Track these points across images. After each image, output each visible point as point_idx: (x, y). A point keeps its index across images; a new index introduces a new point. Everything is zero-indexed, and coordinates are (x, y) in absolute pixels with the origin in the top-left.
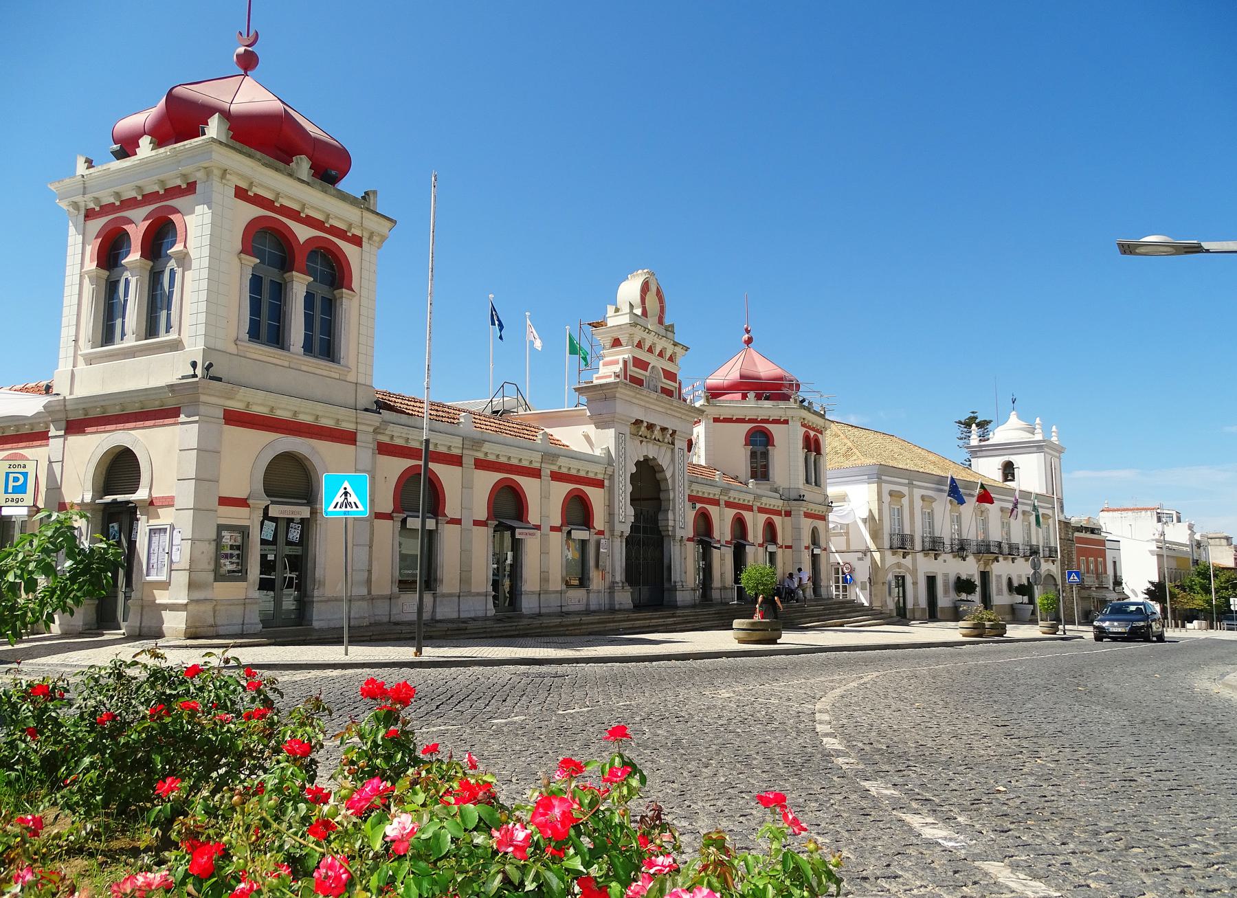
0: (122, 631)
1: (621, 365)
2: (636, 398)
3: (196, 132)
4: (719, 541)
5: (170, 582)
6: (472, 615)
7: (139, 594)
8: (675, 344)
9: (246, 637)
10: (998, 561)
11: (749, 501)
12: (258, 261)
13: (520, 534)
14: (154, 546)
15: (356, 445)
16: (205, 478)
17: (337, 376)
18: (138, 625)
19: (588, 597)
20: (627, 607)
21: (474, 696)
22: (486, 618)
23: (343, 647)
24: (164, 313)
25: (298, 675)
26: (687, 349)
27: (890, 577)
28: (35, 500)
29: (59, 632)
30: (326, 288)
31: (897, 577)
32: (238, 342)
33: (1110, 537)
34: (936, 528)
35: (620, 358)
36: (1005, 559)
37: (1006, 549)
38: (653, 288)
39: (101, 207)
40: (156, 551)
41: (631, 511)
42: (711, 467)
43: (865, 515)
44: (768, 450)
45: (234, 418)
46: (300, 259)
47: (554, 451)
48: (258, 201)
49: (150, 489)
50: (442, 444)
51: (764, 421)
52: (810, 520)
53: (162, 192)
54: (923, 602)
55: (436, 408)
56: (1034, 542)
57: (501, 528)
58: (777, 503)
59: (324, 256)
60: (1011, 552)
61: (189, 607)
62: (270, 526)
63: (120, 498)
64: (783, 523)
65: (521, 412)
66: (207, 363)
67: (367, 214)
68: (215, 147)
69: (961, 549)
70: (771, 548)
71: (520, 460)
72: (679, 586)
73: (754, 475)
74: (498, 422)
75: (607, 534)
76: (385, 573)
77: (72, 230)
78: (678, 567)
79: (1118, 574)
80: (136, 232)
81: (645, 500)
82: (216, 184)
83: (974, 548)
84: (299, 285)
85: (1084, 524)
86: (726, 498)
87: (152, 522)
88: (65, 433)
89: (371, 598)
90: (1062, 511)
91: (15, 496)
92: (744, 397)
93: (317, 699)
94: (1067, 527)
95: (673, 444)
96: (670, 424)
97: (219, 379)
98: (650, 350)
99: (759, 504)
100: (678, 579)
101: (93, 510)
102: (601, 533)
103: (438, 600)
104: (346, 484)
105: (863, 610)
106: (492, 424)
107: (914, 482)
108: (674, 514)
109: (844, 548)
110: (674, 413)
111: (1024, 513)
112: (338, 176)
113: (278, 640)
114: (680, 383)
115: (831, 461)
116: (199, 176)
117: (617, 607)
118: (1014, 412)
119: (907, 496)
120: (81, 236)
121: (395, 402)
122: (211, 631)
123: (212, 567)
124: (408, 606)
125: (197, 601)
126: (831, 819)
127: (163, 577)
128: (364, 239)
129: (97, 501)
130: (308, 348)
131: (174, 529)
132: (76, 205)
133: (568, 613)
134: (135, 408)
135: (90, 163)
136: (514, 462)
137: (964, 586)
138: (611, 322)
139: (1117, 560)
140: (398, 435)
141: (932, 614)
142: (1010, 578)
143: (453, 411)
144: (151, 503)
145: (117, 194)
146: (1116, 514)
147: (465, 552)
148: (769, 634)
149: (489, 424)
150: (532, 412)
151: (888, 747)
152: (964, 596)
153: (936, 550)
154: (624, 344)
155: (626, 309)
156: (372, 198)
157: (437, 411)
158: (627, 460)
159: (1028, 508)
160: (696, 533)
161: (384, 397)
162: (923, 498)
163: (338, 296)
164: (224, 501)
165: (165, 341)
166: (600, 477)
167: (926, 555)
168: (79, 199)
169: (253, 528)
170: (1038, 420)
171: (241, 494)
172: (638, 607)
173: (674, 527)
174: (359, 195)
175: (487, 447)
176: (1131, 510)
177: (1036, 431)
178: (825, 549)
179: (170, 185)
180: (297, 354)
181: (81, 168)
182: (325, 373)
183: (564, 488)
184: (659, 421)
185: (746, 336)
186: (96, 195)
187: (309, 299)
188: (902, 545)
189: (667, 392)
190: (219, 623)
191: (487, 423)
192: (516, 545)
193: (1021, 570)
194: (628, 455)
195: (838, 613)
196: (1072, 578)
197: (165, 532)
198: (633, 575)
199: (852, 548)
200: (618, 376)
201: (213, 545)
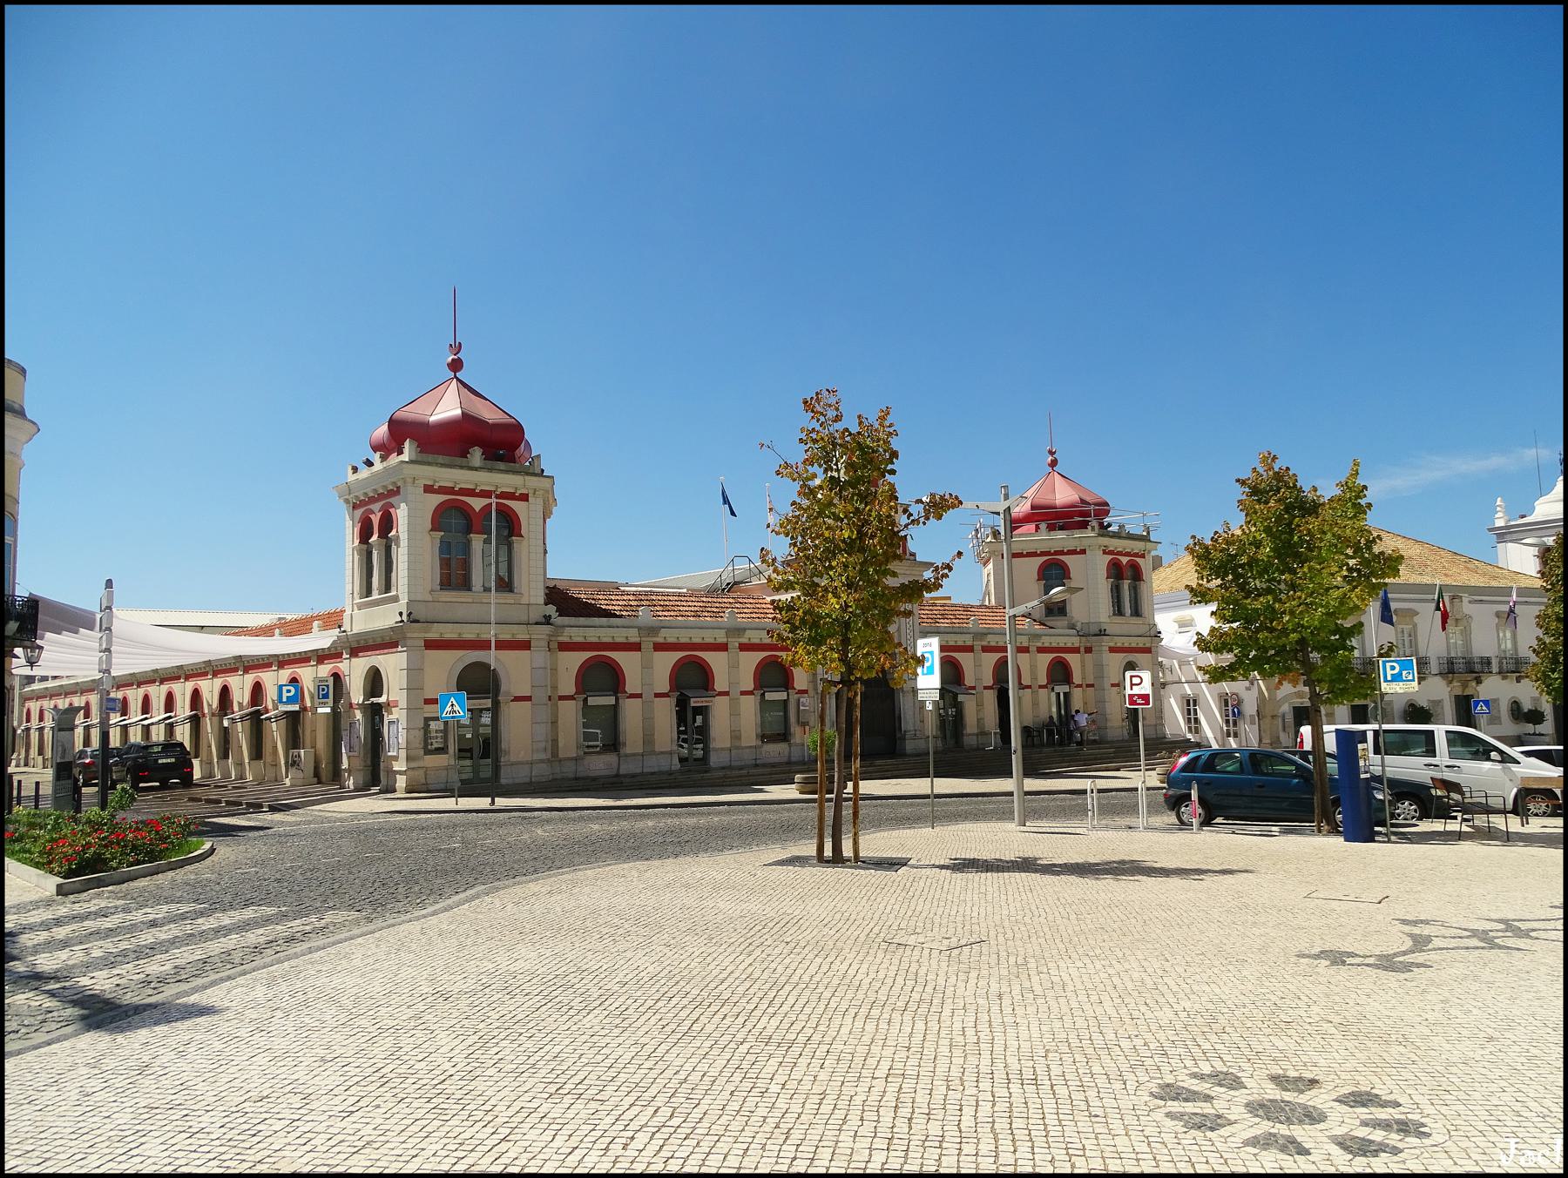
9: (447, 791)
17: (513, 602)
22: (670, 773)
34: (1420, 639)
45: (431, 645)
48: (1111, 553)
51: (1057, 553)
58: (1074, 641)
61: (408, 773)
64: (1083, 662)
67: (527, 478)
80: (376, 519)
82: (410, 489)
97: (418, 621)
122: (424, 788)
124: (775, 751)
127: (395, 754)
134: (379, 641)
144: (389, 705)
180: (479, 592)
196: (1479, 708)
201: (422, 731)
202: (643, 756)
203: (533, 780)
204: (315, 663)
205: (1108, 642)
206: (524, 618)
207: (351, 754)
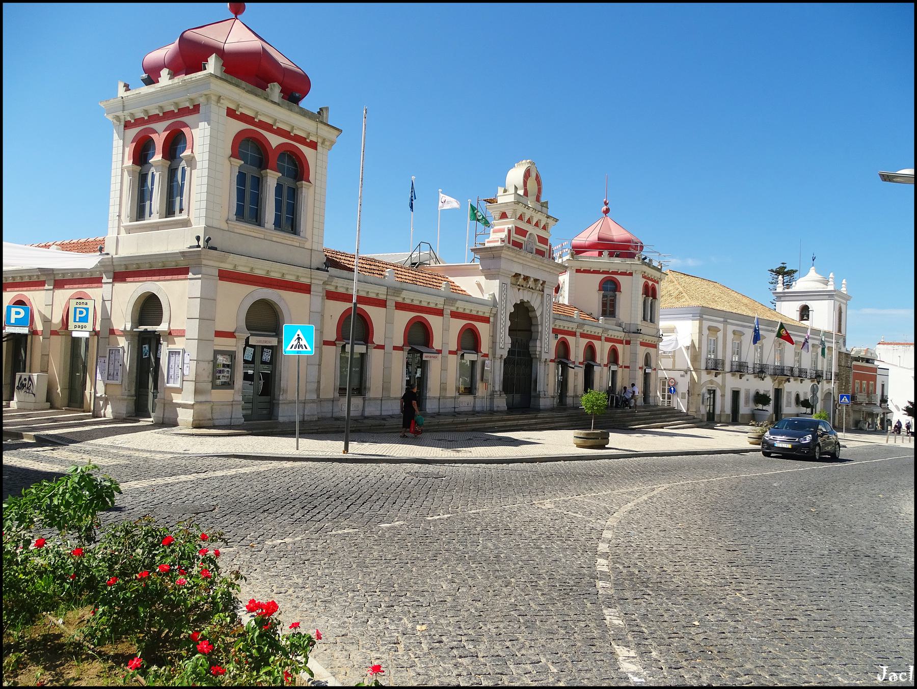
0: (151, 419)
1: (506, 233)
2: (517, 258)
3: (200, 67)
4: (574, 363)
5: (182, 389)
6: (390, 413)
7: (162, 397)
8: (548, 217)
10: (789, 382)
11: (598, 333)
12: (243, 162)
13: (426, 357)
14: (172, 363)
15: (310, 293)
16: (205, 318)
17: (298, 244)
18: (162, 416)
19: (475, 402)
20: (502, 409)
21: (374, 498)
23: (295, 439)
24: (178, 199)
25: (263, 466)
26: (557, 220)
27: (704, 390)
28: (94, 324)
29: (112, 417)
30: (291, 180)
31: (709, 391)
32: (229, 222)
33: (881, 365)
35: (506, 227)
36: (795, 380)
37: (796, 373)
38: (533, 175)
39: (135, 120)
40: (173, 367)
41: (509, 340)
42: (572, 306)
43: (689, 344)
44: (616, 295)
45: (225, 276)
46: (273, 159)
47: (456, 294)
48: (243, 118)
49: (169, 324)
50: (373, 292)
52: (644, 348)
53: (176, 111)
54: (728, 410)
55: (370, 262)
56: (819, 368)
57: (413, 351)
58: (620, 335)
59: (290, 157)
60: (801, 375)
61: (195, 407)
62: (250, 351)
63: (150, 328)
64: (624, 349)
65: (433, 264)
66: (207, 237)
67: (321, 126)
68: (213, 80)
69: (761, 372)
70: (614, 368)
71: (429, 303)
72: (542, 394)
73: (604, 314)
74: (415, 273)
75: (490, 356)
76: (329, 388)
77: (116, 136)
78: (542, 381)
79: (885, 394)
80: (159, 139)
81: (519, 330)
82: (214, 107)
83: (771, 371)
84: (272, 179)
85: (862, 354)
86: (581, 331)
87: (170, 347)
88: (113, 281)
89: (320, 401)
90: (845, 345)
91: (81, 324)
92: (600, 254)
93: (237, 572)
94: (847, 357)
95: (543, 291)
96: (541, 276)
97: (215, 249)
98: (529, 221)
99: (606, 335)
100: (542, 390)
101: (132, 335)
102: (486, 355)
103: (367, 402)
104: (299, 332)
105: (680, 416)
106: (410, 275)
107: (728, 320)
108: (541, 342)
109: (671, 367)
110: (545, 269)
111: (813, 345)
112: (301, 97)
113: (254, 431)
114: (550, 246)
115: (664, 302)
116: (202, 100)
117: (495, 409)
118: (813, 268)
119: (722, 331)
120: (122, 141)
121: (340, 259)
122: (210, 423)
123: (210, 379)
125: (201, 402)
126: (567, 648)
127: (178, 385)
128: (318, 143)
129: (135, 330)
130: (278, 225)
131: (185, 352)
132: (118, 118)
133: (459, 413)
134: (159, 266)
135: (127, 88)
136: (424, 304)
137: (761, 399)
138: (501, 200)
139: (885, 383)
140: (340, 286)
141: (735, 419)
142: (798, 395)
143: (382, 265)
144: (170, 333)
145: (146, 111)
146: (890, 347)
147: (387, 369)
148: (599, 441)
149: (408, 274)
150: (442, 265)
151: (639, 571)
152: (760, 406)
153: (741, 372)
154: (509, 217)
155: (512, 191)
156: (325, 112)
157: (370, 265)
158: (508, 303)
159: (817, 342)
160: (557, 356)
161: (333, 255)
162: (734, 332)
163: (299, 186)
164: (219, 334)
165: (179, 220)
166: (487, 315)
167: (733, 375)
168: (120, 114)
169: (238, 352)
170: (831, 275)
171: (230, 329)
172: (512, 408)
173: (540, 352)
174: (315, 111)
175: (404, 294)
176: (902, 344)
177: (829, 283)
178: (655, 369)
179: (182, 106)
180: (270, 230)
181: (121, 92)
182: (289, 242)
183: (460, 323)
184: (533, 275)
185: (605, 208)
186: (131, 111)
187: (279, 188)
188: (715, 367)
189: (540, 253)
190: (215, 418)
191: (406, 274)
192: (423, 365)
193: (804, 388)
194: (508, 299)
195: (661, 418)
196: (843, 400)
197: (179, 354)
198: (508, 386)
199: (677, 368)
200: (503, 241)
201: (211, 365)
202: (333, 401)
203: (306, 419)
204: (52, 287)
205: (640, 338)
206: (307, 263)
207: (109, 382)
